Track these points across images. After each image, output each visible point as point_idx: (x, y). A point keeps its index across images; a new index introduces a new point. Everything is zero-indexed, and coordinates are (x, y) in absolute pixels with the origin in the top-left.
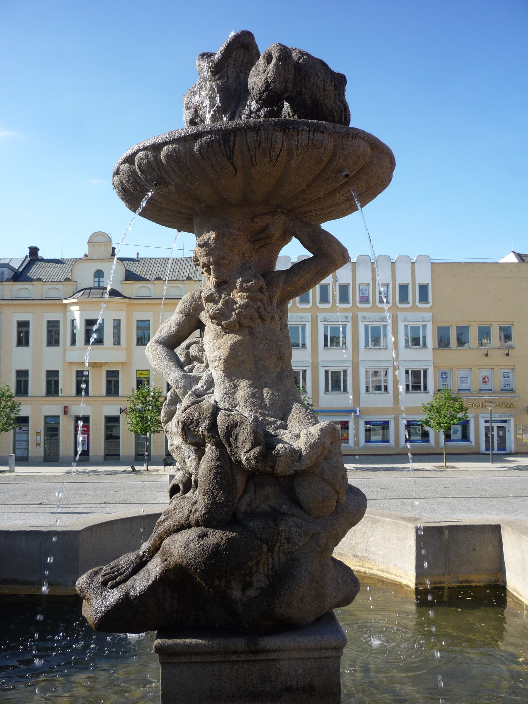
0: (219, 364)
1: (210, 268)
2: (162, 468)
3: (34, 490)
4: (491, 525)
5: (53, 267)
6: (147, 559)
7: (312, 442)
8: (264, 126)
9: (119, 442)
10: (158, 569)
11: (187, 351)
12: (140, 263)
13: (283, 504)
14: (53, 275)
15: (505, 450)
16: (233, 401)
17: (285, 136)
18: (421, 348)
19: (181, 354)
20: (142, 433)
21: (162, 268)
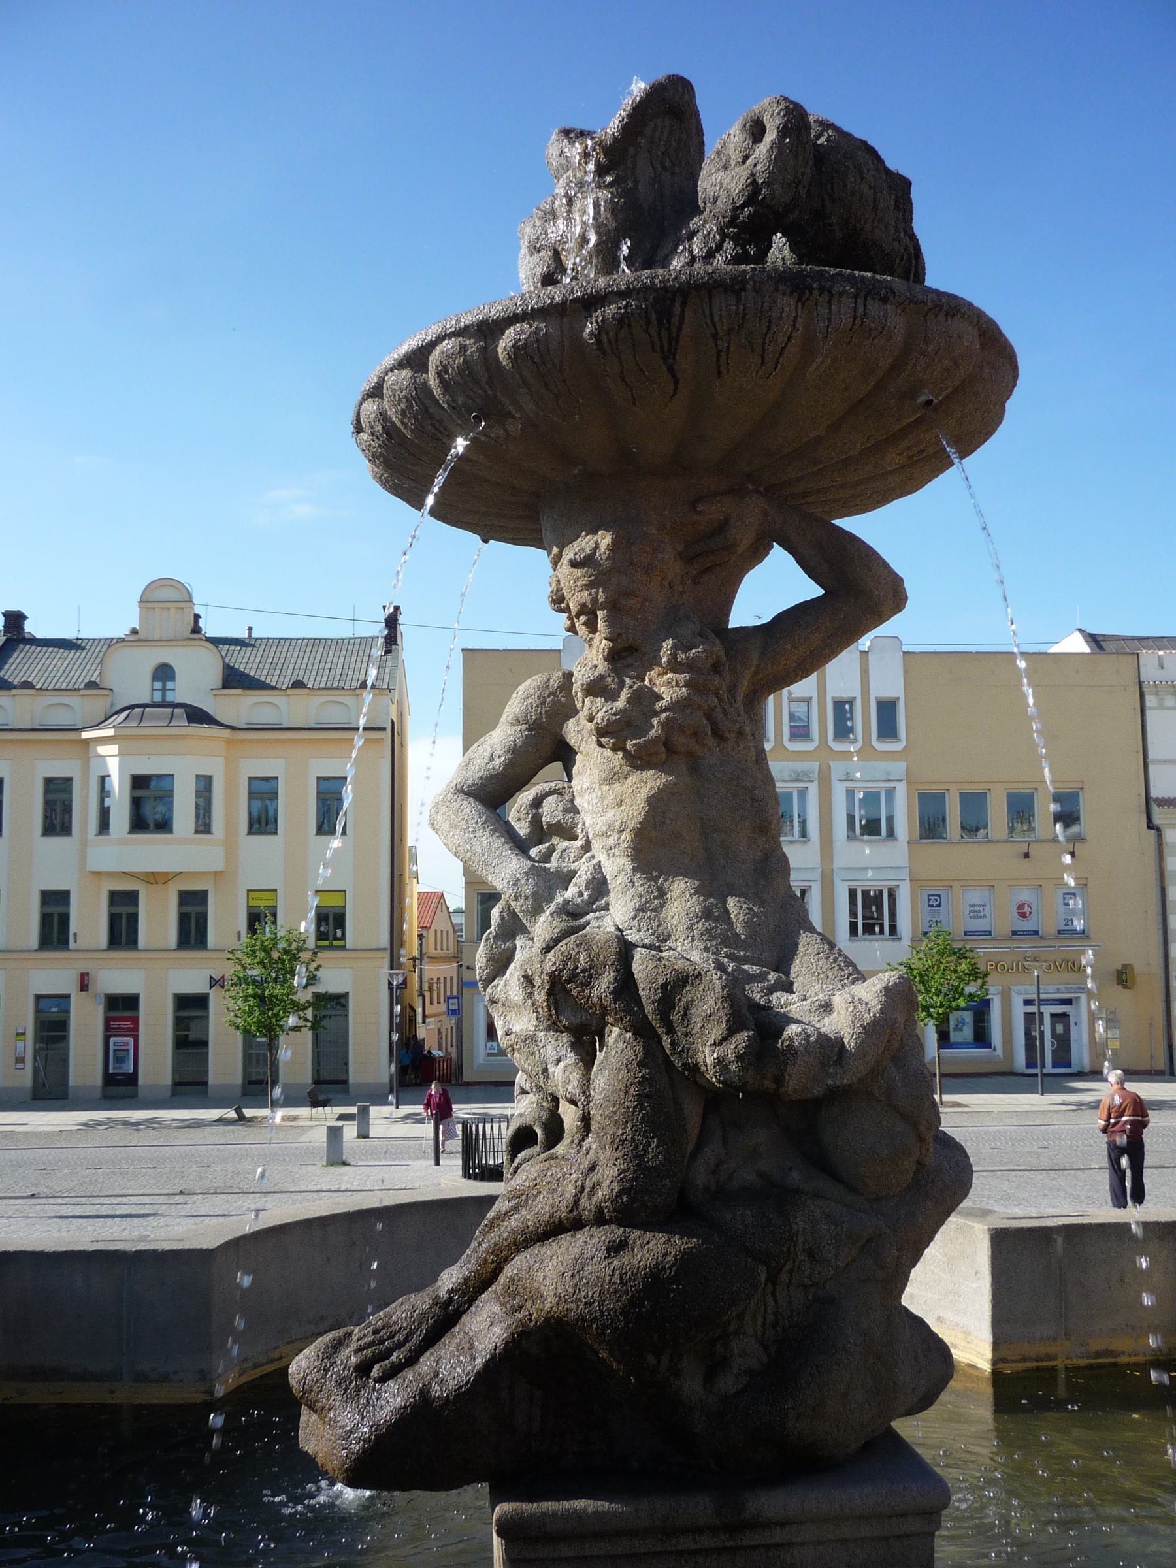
0: (621, 841)
1: (597, 617)
2: (304, 1112)
3: (13, 1165)
4: (1157, 1223)
5: (58, 657)
6: (458, 1307)
7: (868, 1018)
8: (755, 282)
9: (207, 1054)
10: (497, 1330)
11: (534, 811)
12: (255, 649)
13: (791, 1169)
14: (59, 674)
15: (1069, 1065)
16: (659, 926)
17: (800, 305)
18: (883, 841)
19: (519, 819)
20: (261, 1032)
21: (305, 661)
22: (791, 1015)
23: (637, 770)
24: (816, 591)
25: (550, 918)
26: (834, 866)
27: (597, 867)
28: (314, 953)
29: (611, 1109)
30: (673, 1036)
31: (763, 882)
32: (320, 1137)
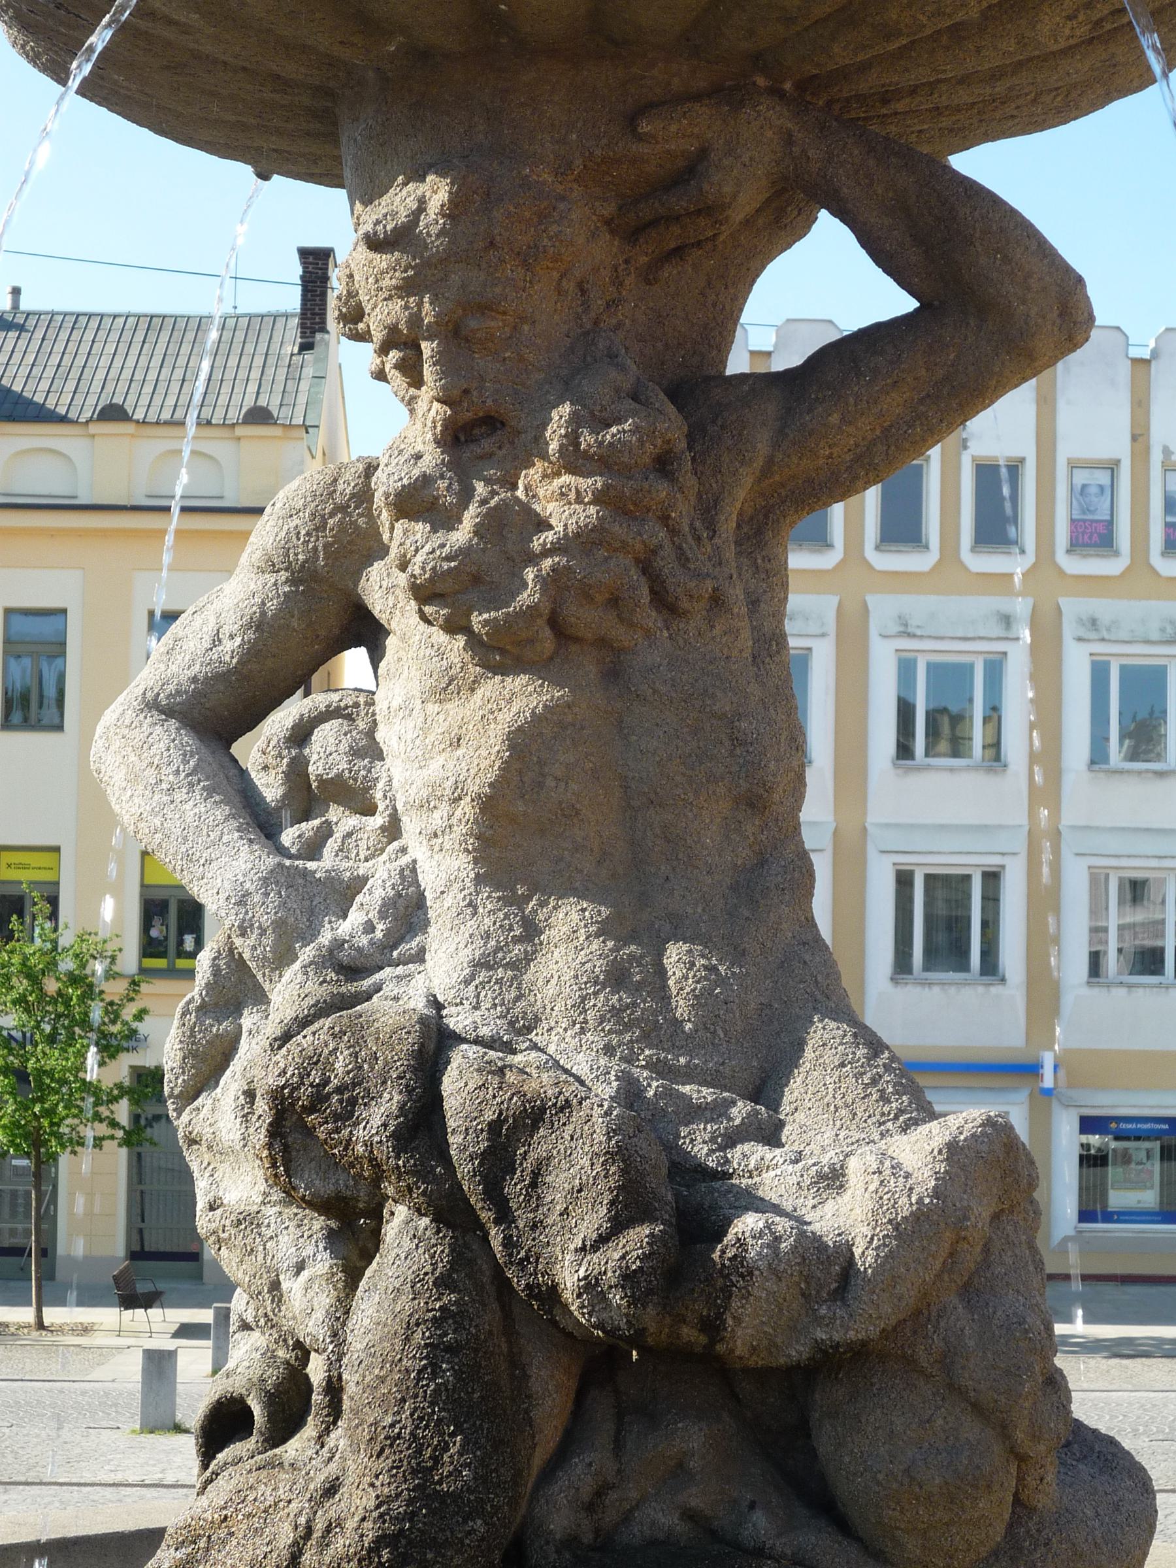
1: (420, 352)
7: (905, 1207)
13: (752, 1506)
16: (518, 999)
19: (265, 768)
20: (17, 1147)
22: (760, 1193)
23: (495, 674)
24: (906, 304)
25: (300, 975)
26: (869, 820)
27: (407, 872)
28: (134, 983)
29: (377, 1371)
30: (509, 1227)
31: (746, 913)
32: (131, 1369)
